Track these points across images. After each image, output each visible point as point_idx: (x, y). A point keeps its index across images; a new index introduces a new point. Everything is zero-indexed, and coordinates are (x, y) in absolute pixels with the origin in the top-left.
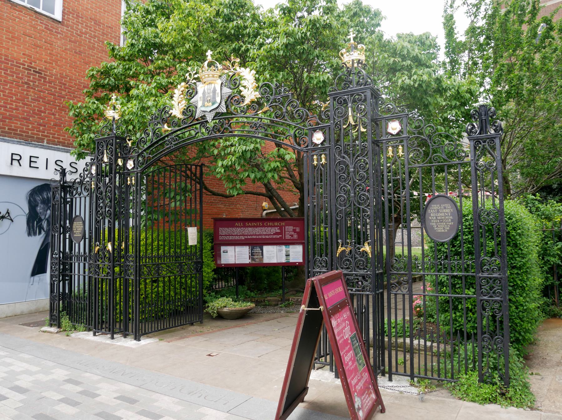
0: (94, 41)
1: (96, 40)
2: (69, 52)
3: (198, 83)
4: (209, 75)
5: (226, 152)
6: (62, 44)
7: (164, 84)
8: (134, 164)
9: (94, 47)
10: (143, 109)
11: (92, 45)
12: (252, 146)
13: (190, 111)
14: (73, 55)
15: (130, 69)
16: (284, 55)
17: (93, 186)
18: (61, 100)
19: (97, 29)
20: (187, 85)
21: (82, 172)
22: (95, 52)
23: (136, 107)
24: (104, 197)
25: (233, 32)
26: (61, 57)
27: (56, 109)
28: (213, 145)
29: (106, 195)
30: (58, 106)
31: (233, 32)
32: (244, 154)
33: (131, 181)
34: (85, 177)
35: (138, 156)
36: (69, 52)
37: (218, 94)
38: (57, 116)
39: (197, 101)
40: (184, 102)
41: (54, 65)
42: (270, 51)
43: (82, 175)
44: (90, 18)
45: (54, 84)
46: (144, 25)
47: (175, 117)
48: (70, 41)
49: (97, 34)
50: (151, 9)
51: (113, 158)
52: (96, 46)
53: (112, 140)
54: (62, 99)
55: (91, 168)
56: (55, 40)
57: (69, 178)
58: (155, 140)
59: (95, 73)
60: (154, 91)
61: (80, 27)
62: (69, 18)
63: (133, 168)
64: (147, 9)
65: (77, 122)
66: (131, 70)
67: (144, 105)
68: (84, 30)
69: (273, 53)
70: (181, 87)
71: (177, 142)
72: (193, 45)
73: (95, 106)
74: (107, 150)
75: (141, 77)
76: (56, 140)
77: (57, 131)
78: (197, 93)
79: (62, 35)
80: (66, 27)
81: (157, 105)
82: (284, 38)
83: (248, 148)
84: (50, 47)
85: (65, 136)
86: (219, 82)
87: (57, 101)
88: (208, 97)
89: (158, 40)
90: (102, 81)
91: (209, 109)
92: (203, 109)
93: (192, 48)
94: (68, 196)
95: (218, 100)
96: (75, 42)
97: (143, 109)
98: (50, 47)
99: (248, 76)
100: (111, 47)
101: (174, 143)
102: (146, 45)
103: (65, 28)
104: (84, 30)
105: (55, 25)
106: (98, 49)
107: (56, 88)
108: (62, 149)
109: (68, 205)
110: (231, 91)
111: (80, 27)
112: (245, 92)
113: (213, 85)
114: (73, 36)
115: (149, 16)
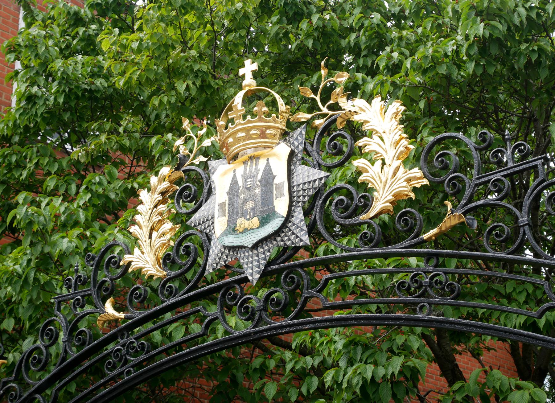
3: (213, 163)
4: (248, 130)
5: (304, 390)
7: (112, 196)
10: (45, 262)
12: (397, 363)
13: (188, 254)
15: (20, 166)
16: (480, 72)
20: (180, 173)
23: (26, 258)
25: (310, 43)
28: (263, 370)
31: (310, 43)
32: (370, 392)
37: (279, 187)
39: (210, 220)
40: (168, 225)
42: (433, 68)
46: (67, 52)
47: (139, 272)
50: (86, 12)
58: (74, 353)
60: (82, 216)
64: (76, 14)
66: (24, 168)
67: (47, 250)
69: (443, 70)
70: (160, 182)
71: (142, 357)
72: (198, 83)
75: (51, 183)
78: (210, 192)
81: (86, 250)
82: (474, 22)
83: (381, 371)
86: (283, 150)
88: (245, 201)
89: (100, 83)
91: (249, 240)
92: (232, 240)
93: (194, 92)
95: (281, 206)
97: (45, 262)
99: (381, 119)
101: (134, 360)
102: (67, 97)
110: (323, 174)
112: (372, 174)
113: (262, 163)
115: (81, 30)
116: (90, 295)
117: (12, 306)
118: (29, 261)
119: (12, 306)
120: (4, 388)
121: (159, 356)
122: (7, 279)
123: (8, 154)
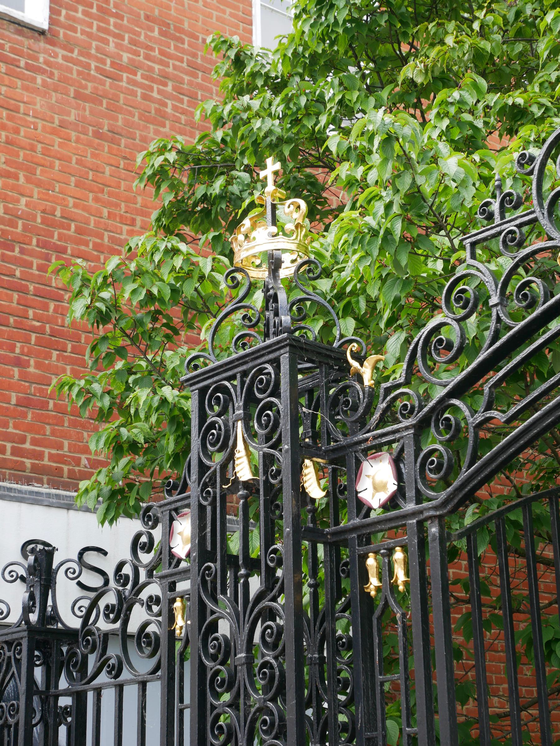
0: (160, 92)
1: (169, 88)
2: (73, 134)
6: (51, 108)
8: (399, 476)
9: (164, 115)
11: (153, 106)
14: (89, 144)
17: (180, 622)
18: (46, 308)
19: (172, 51)
21: (127, 555)
22: (167, 130)
24: (242, 674)
26: (46, 152)
27: (28, 341)
29: (250, 661)
30: (33, 330)
33: (389, 570)
34: (143, 578)
35: (421, 428)
36: (73, 134)
38: (32, 370)
41: (22, 180)
43: (127, 570)
44: (147, 17)
45: (22, 251)
48: (78, 96)
49: (170, 70)
51: (284, 458)
52: (169, 110)
53: (276, 363)
54: (52, 306)
55: (169, 533)
56: (26, 96)
57: (67, 600)
59: (172, 156)
61: (111, 47)
62: (74, 19)
63: (392, 503)
65: (103, 349)
68: (126, 56)
73: (178, 262)
74: (247, 419)
76: (28, 462)
77: (30, 428)
79: (51, 75)
80: (65, 48)
84: (9, 118)
85: (60, 447)
87: (31, 313)
90: (200, 190)
94: (63, 684)
96: (95, 99)
98: (9, 118)
100: (232, 54)
103: (61, 52)
104: (126, 56)
105: (26, 42)
106: (178, 121)
107: (30, 265)
108: (49, 495)
109: (63, 730)
111: (111, 47)
114: (88, 77)
116: (535, 220)
117: (347, 299)
118: (388, 207)
119: (347, 299)
120: (388, 398)
121: (543, 400)
122: (355, 239)
123: (293, 95)
